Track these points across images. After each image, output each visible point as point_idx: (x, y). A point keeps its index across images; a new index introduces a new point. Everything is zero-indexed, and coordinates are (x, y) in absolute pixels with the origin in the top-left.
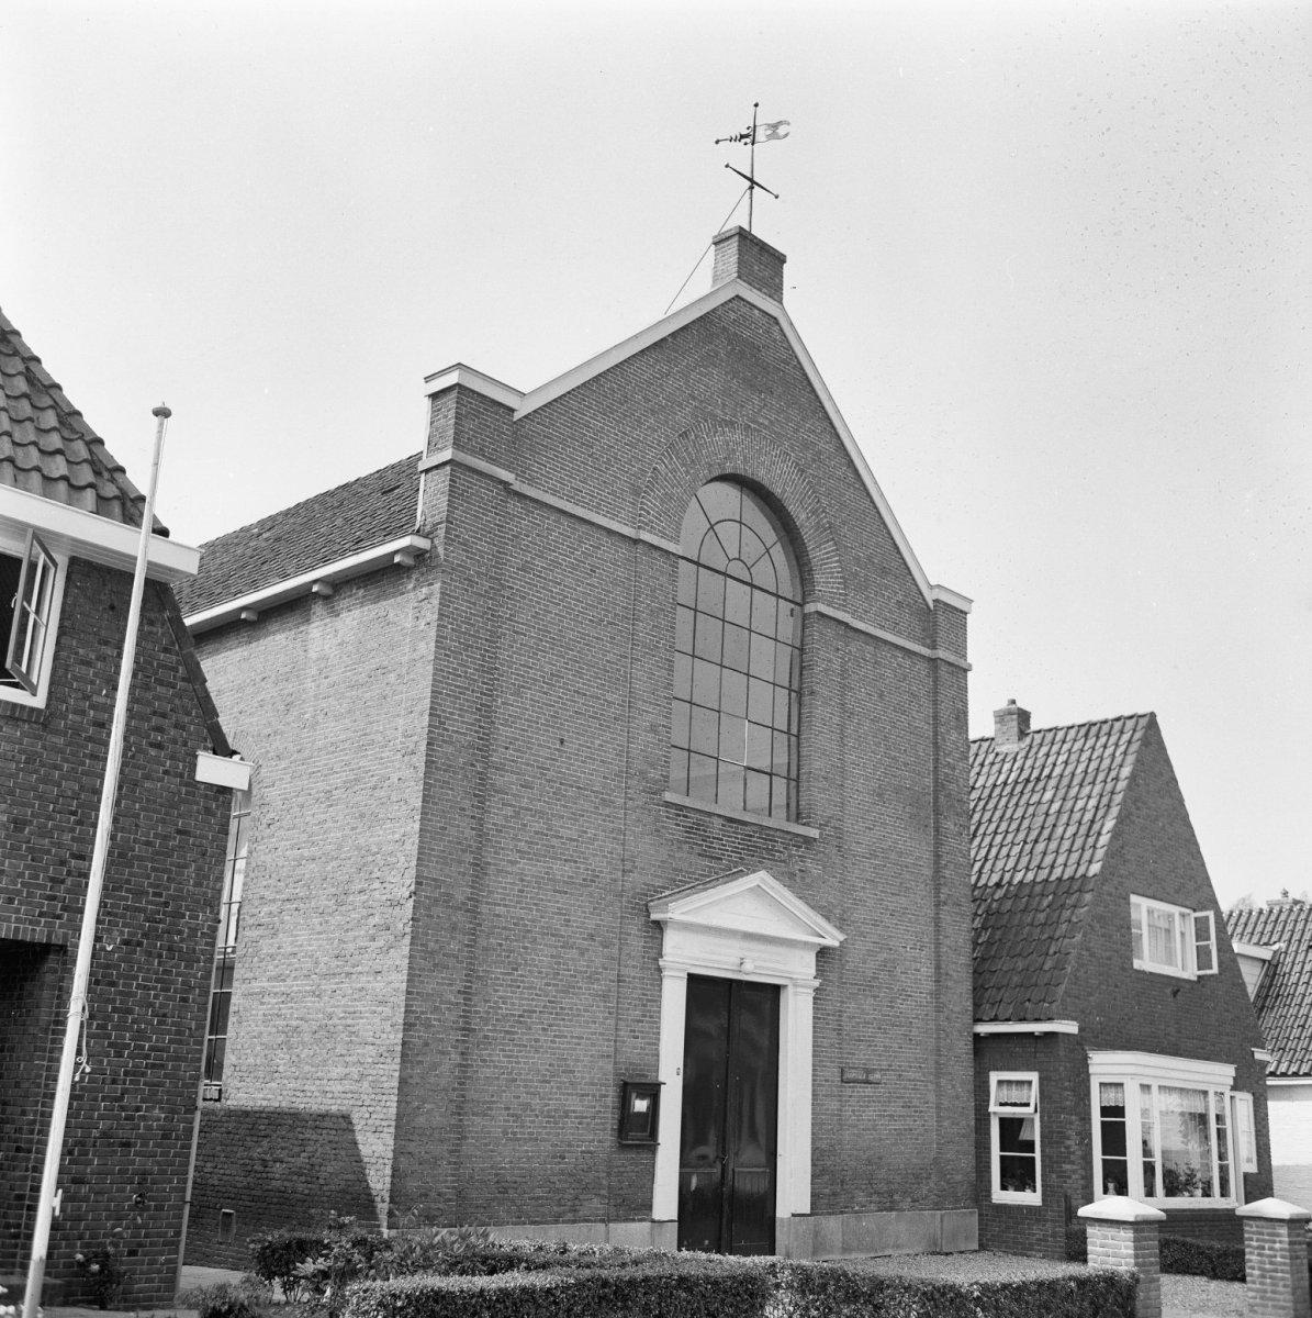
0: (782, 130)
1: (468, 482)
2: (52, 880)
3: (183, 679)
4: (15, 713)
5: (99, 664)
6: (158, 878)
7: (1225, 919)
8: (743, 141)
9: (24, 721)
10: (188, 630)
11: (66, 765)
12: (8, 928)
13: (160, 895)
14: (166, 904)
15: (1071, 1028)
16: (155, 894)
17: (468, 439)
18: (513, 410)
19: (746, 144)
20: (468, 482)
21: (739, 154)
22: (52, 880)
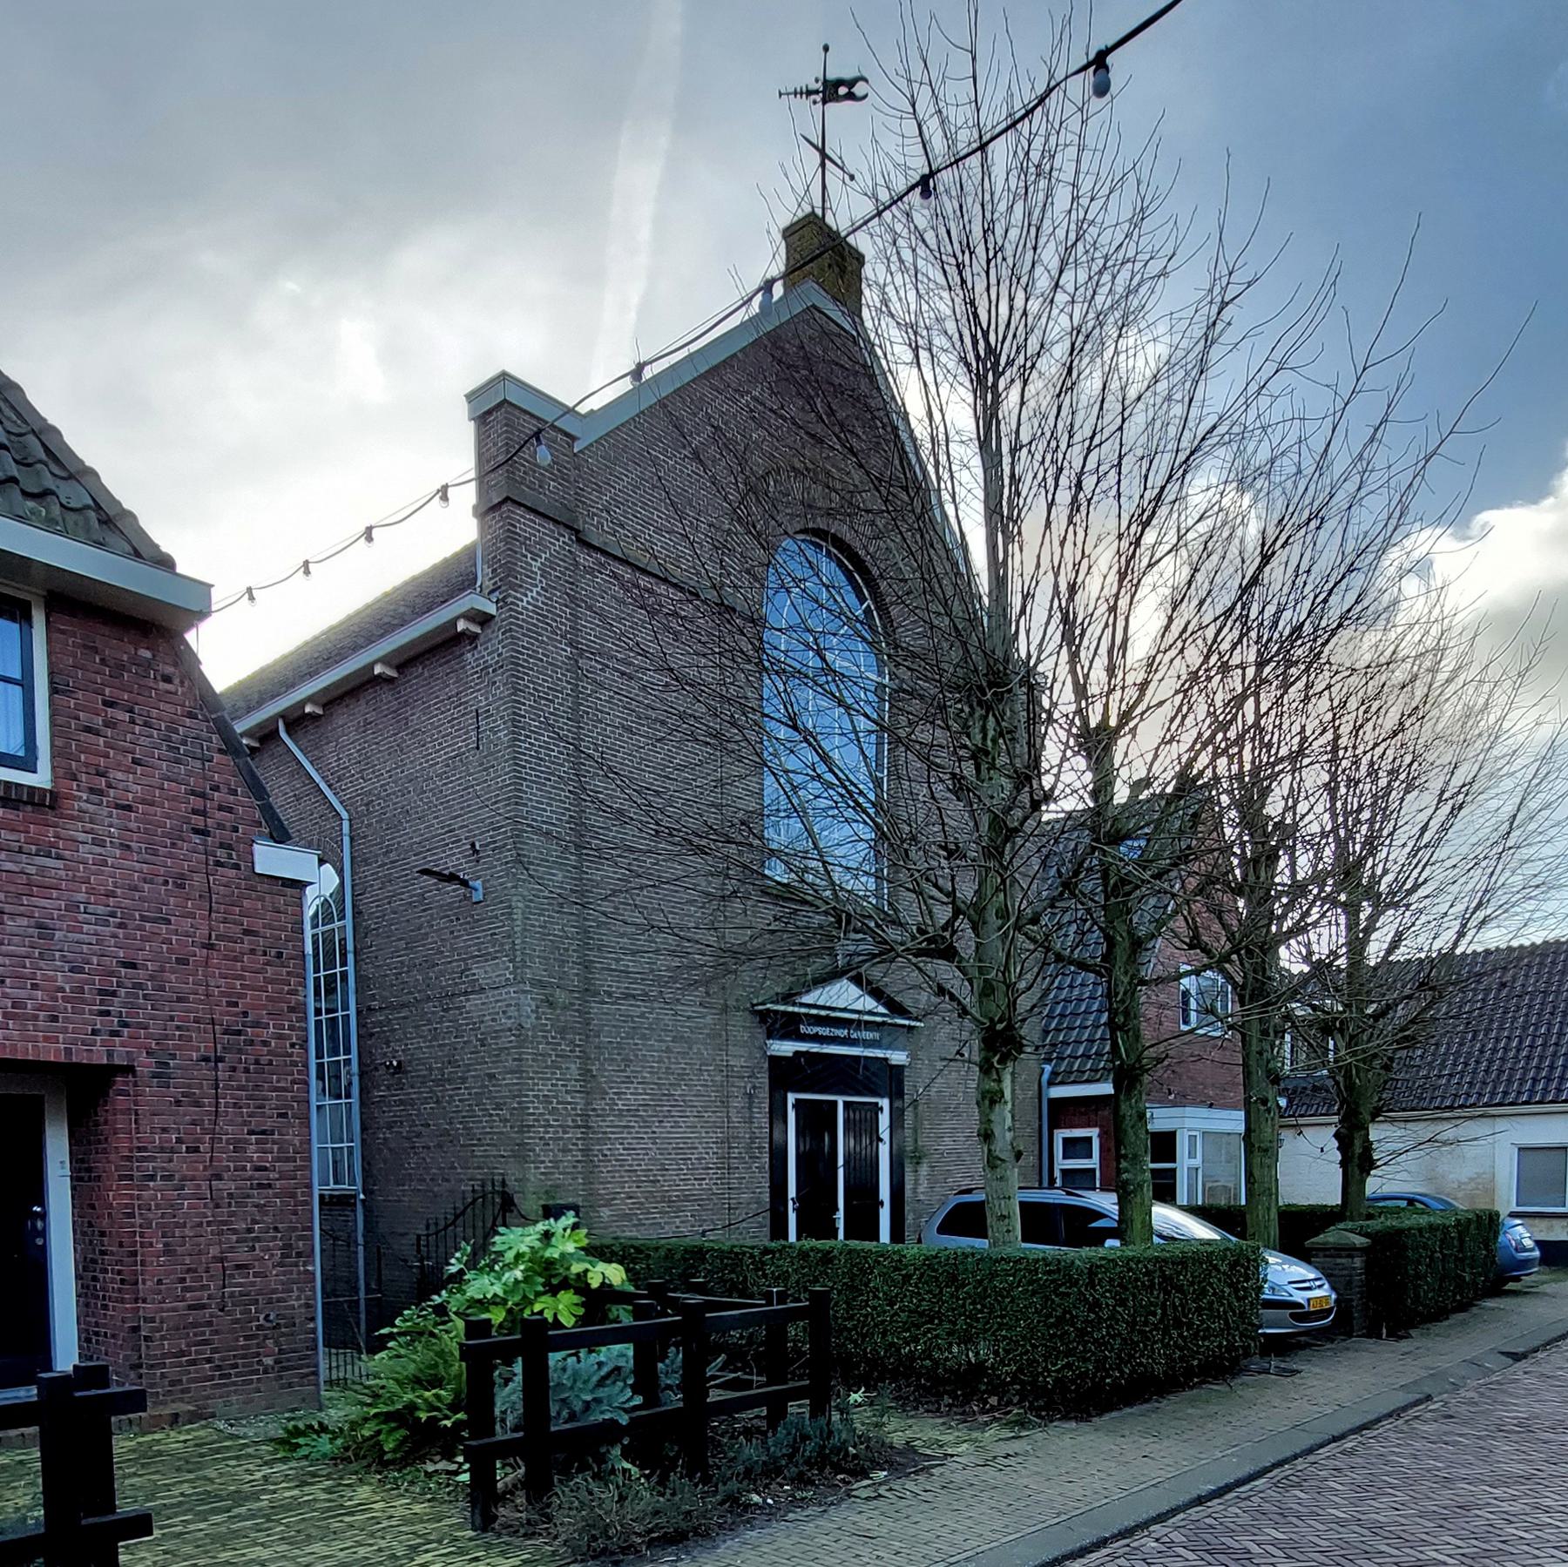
0: (859, 89)
1: (530, 527)
2: (101, 992)
3: (220, 751)
4: (11, 797)
5: (109, 732)
6: (228, 986)
7: (760, 294)
8: (813, 97)
9: (26, 803)
10: (227, 704)
11: (172, 899)
12: (57, 1050)
13: (236, 1004)
14: (245, 1014)
15: (1166, 1220)
16: (230, 1004)
17: (525, 473)
18: (574, 438)
19: (815, 102)
20: (530, 527)
21: (808, 110)
22: (101, 992)
